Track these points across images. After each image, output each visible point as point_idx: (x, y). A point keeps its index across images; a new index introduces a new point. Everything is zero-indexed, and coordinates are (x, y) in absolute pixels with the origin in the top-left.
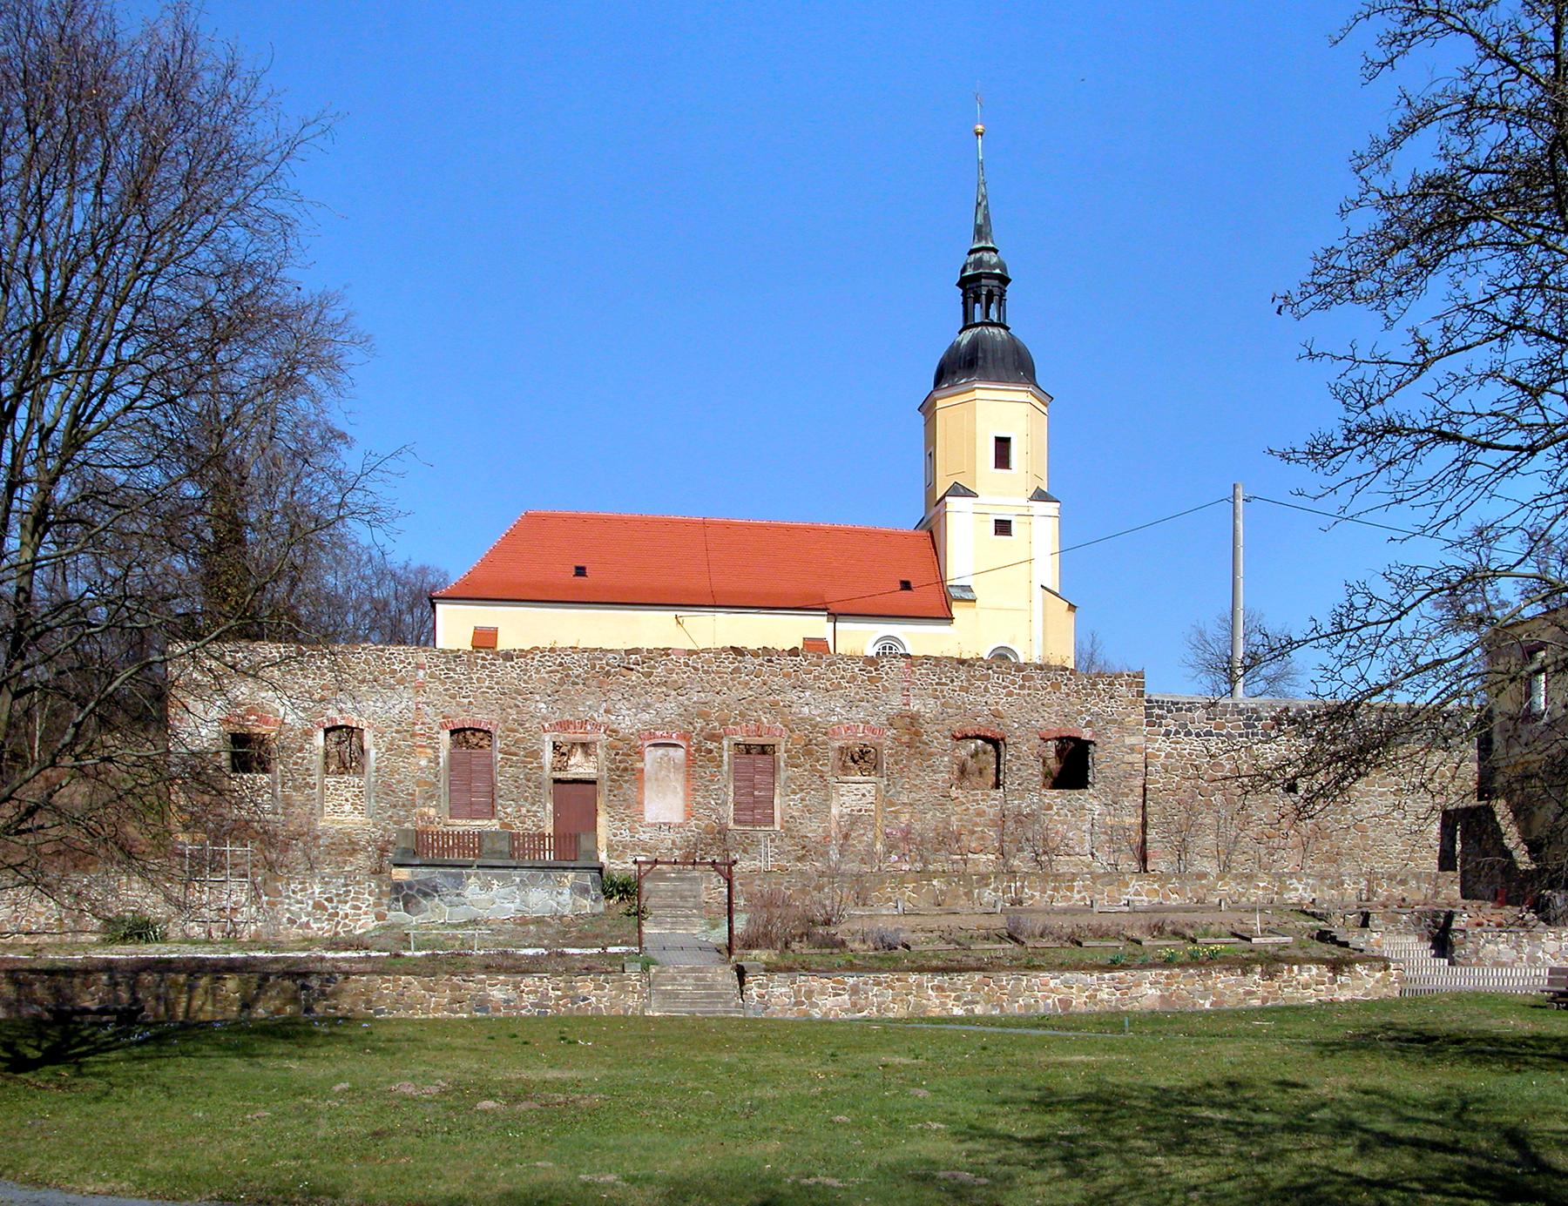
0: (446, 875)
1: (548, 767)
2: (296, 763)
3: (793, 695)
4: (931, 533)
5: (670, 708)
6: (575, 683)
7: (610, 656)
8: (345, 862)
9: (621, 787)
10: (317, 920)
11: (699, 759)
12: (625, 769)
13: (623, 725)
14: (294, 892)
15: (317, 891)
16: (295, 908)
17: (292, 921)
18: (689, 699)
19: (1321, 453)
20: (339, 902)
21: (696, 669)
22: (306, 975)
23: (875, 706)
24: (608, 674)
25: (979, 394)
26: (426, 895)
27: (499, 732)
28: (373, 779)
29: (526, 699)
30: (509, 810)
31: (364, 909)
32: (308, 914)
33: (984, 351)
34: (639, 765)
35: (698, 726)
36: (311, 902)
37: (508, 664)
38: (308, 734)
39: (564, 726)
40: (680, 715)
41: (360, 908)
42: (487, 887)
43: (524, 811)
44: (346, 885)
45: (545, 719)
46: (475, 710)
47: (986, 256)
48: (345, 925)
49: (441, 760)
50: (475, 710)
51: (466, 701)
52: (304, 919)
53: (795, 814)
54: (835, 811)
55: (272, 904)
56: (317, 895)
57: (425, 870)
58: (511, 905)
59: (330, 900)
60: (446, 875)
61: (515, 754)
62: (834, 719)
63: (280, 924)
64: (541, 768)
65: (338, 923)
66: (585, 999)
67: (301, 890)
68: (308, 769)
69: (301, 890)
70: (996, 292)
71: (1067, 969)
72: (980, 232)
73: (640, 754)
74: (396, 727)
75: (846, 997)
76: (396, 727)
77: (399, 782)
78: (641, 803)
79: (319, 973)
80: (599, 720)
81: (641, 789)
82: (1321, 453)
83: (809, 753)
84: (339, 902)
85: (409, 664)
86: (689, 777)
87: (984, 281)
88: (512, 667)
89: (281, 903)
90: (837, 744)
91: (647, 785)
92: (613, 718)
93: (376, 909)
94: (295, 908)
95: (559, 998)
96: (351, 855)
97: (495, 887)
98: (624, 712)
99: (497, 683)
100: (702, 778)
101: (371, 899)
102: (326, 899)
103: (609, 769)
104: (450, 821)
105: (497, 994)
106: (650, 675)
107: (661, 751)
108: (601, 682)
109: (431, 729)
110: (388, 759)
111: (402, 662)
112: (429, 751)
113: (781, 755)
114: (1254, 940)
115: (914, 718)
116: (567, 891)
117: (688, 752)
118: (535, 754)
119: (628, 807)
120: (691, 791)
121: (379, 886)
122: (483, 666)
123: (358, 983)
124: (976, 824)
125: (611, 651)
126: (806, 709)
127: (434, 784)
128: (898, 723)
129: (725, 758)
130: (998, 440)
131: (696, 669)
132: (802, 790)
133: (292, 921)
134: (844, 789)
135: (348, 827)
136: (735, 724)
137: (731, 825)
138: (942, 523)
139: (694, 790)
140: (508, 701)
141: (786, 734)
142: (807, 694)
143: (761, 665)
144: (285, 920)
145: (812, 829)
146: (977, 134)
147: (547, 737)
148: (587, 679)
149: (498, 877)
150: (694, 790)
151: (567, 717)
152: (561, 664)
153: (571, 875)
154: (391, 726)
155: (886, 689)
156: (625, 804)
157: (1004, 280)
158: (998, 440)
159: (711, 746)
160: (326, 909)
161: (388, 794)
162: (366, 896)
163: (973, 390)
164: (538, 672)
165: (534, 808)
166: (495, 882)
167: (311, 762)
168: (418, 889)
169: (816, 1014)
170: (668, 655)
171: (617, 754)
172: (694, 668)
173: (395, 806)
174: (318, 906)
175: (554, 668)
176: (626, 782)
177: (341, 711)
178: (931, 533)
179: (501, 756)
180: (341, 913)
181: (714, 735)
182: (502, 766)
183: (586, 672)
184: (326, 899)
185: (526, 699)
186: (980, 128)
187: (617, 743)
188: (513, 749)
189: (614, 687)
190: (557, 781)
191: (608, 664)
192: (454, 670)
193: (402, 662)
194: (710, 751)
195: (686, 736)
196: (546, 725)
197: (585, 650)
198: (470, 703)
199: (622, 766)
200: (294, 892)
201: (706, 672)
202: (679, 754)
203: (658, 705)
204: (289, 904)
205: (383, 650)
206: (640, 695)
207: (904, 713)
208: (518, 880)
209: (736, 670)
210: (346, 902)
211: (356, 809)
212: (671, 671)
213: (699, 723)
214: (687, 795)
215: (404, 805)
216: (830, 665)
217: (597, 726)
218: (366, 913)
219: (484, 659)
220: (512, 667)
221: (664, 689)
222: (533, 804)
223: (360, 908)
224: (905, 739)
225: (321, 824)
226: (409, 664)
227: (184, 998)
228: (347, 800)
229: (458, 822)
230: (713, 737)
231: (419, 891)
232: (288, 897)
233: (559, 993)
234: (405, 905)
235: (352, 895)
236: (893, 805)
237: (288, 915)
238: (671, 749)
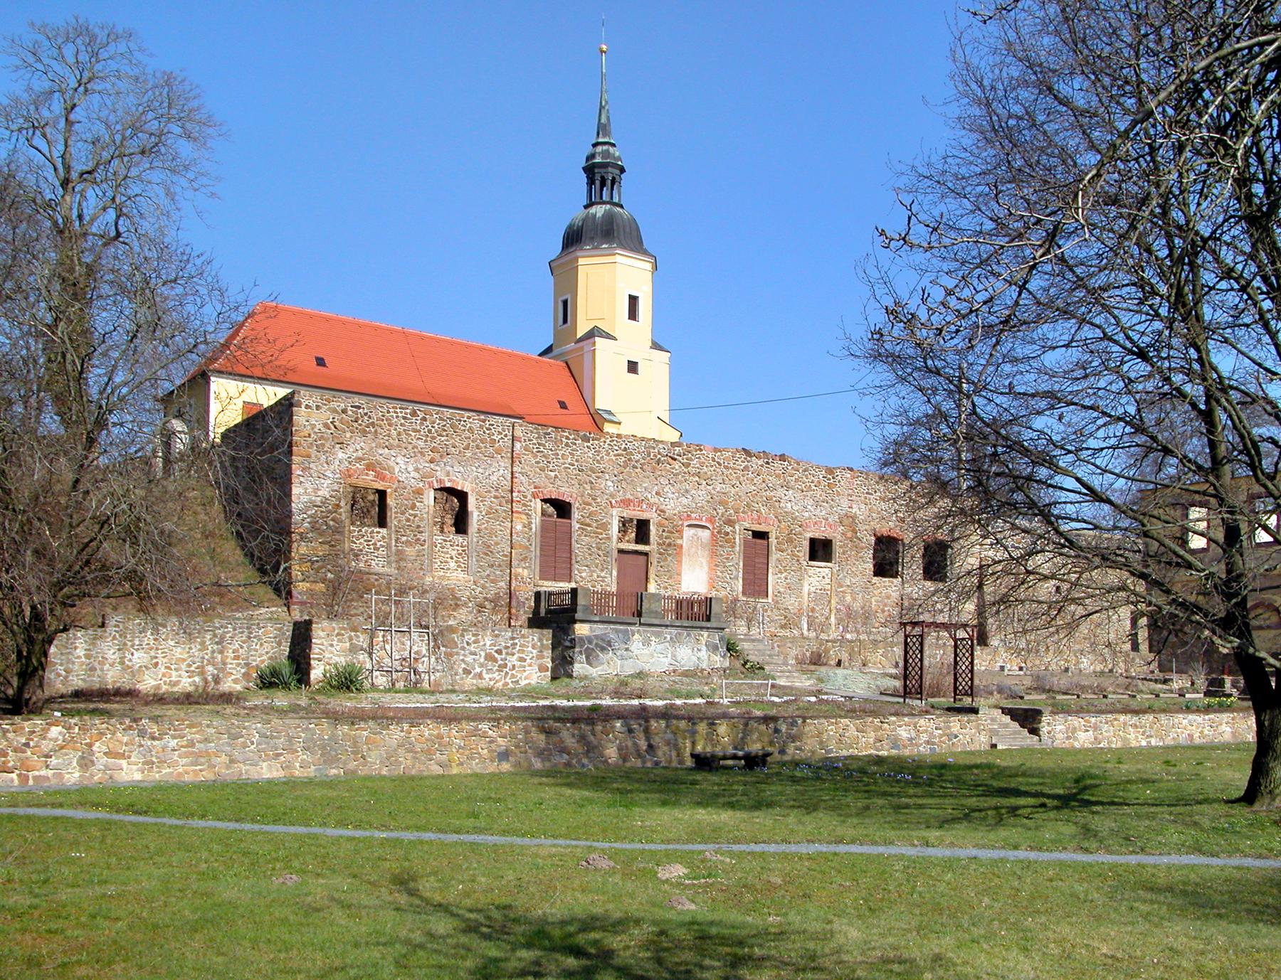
0: (617, 631)
1: (615, 538)
2: (408, 520)
3: (780, 492)
4: (567, 363)
5: (701, 495)
6: (635, 467)
7: (661, 446)
8: (450, 616)
9: (666, 559)
10: (489, 671)
11: (720, 539)
12: (669, 545)
13: (669, 507)
14: (468, 644)
15: (488, 643)
16: (469, 659)
17: (466, 672)
18: (714, 489)
19: (609, 336)
20: (507, 654)
21: (720, 464)
22: (774, 719)
23: (832, 507)
24: (658, 462)
25: (618, 258)
26: (603, 649)
27: (577, 505)
28: (475, 540)
29: (598, 478)
30: (584, 575)
31: (528, 661)
32: (481, 665)
33: (618, 225)
34: (679, 542)
35: (720, 512)
36: (483, 654)
37: (586, 444)
38: (419, 492)
39: (626, 503)
40: (708, 502)
41: (525, 660)
42: (646, 643)
43: (595, 575)
44: (513, 638)
45: (612, 496)
46: (560, 483)
47: (611, 149)
48: (513, 676)
49: (533, 526)
50: (560, 483)
51: (553, 474)
52: (478, 670)
53: (782, 590)
54: (806, 589)
55: (449, 655)
56: (487, 647)
57: (601, 626)
58: (665, 660)
59: (499, 652)
60: (617, 631)
61: (589, 525)
62: (806, 514)
63: (456, 674)
64: (609, 538)
65: (507, 673)
66: (956, 737)
67: (475, 642)
68: (419, 527)
69: (475, 642)
70: (617, 178)
71: (1193, 712)
72: (602, 129)
73: (680, 532)
74: (494, 493)
75: (1091, 733)
76: (494, 493)
77: (497, 544)
78: (679, 574)
79: (785, 718)
80: (652, 500)
81: (680, 562)
82: (609, 336)
83: (790, 541)
84: (507, 654)
85: (506, 436)
86: (713, 554)
87: (610, 169)
88: (588, 447)
89: (458, 654)
90: (809, 535)
91: (685, 559)
92: (662, 499)
93: (540, 661)
94: (469, 659)
95: (941, 736)
96: (454, 610)
97: (653, 643)
98: (670, 495)
99: (577, 461)
100: (722, 555)
101: (535, 651)
102: (496, 651)
103: (658, 544)
104: (541, 582)
105: (904, 733)
106: (687, 465)
107: (693, 531)
108: (654, 468)
109: (524, 496)
110: (488, 522)
111: (500, 433)
112: (524, 517)
113: (773, 540)
114: (1187, 696)
115: (854, 518)
116: (704, 648)
117: (713, 534)
118: (604, 526)
119: (670, 577)
120: (713, 567)
121: (540, 640)
122: (567, 445)
123: (812, 726)
124: (885, 605)
125: (662, 442)
126: (789, 505)
127: (527, 548)
128: (846, 522)
129: (737, 540)
130: (630, 296)
131: (720, 464)
132: (786, 570)
133: (466, 672)
134: (811, 571)
135: (451, 583)
136: (743, 512)
137: (741, 598)
138: (587, 358)
139: (716, 565)
140: (583, 477)
141: (776, 523)
142: (791, 492)
143: (762, 466)
144: (460, 671)
145: (791, 603)
146: (602, 52)
147: (615, 512)
148: (644, 464)
149: (654, 633)
150: (716, 565)
151: (629, 496)
152: (625, 449)
153: (706, 634)
154: (490, 492)
155: (839, 494)
156: (668, 574)
157: (622, 170)
158: (630, 296)
159: (728, 529)
160: (496, 660)
161: (487, 554)
162: (530, 649)
163: (614, 254)
164: (608, 454)
165: (603, 574)
166: (653, 638)
167: (422, 520)
168: (596, 644)
169: (1077, 745)
170: (701, 450)
171: (664, 531)
172: (718, 463)
173: (492, 566)
174: (489, 657)
175: (620, 452)
176: (669, 555)
177: (448, 474)
178: (567, 363)
179: (578, 526)
180: (509, 664)
181: (730, 520)
182: (579, 535)
183: (644, 459)
184: (496, 651)
185: (598, 478)
186: (604, 48)
187: (664, 521)
188: (588, 521)
189: (663, 473)
190: (621, 551)
191: (659, 453)
192: (544, 446)
193: (500, 433)
194: (727, 534)
195: (711, 520)
196: (613, 502)
197: (643, 439)
198: (556, 477)
199: (667, 541)
200: (468, 644)
201: (726, 467)
202: (705, 534)
203: (694, 492)
204: (465, 655)
205: (484, 421)
206: (681, 482)
207: (849, 514)
208: (669, 637)
209: (746, 468)
210: (513, 654)
211: (459, 566)
212: (702, 464)
213: (721, 510)
214: (711, 569)
215: (500, 566)
216: (805, 471)
217: (650, 505)
218: (530, 665)
219: (567, 438)
220: (588, 447)
221: (697, 479)
222: (602, 570)
223: (525, 660)
224: (849, 534)
225: (428, 579)
226: (506, 436)
227: (688, 744)
228: (452, 558)
229: (546, 583)
230: (730, 522)
231: (597, 645)
232: (463, 649)
233: (940, 732)
234: (587, 658)
235: (518, 648)
236: (842, 586)
237: (463, 666)
238: (700, 530)
